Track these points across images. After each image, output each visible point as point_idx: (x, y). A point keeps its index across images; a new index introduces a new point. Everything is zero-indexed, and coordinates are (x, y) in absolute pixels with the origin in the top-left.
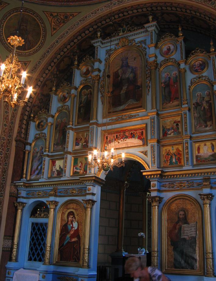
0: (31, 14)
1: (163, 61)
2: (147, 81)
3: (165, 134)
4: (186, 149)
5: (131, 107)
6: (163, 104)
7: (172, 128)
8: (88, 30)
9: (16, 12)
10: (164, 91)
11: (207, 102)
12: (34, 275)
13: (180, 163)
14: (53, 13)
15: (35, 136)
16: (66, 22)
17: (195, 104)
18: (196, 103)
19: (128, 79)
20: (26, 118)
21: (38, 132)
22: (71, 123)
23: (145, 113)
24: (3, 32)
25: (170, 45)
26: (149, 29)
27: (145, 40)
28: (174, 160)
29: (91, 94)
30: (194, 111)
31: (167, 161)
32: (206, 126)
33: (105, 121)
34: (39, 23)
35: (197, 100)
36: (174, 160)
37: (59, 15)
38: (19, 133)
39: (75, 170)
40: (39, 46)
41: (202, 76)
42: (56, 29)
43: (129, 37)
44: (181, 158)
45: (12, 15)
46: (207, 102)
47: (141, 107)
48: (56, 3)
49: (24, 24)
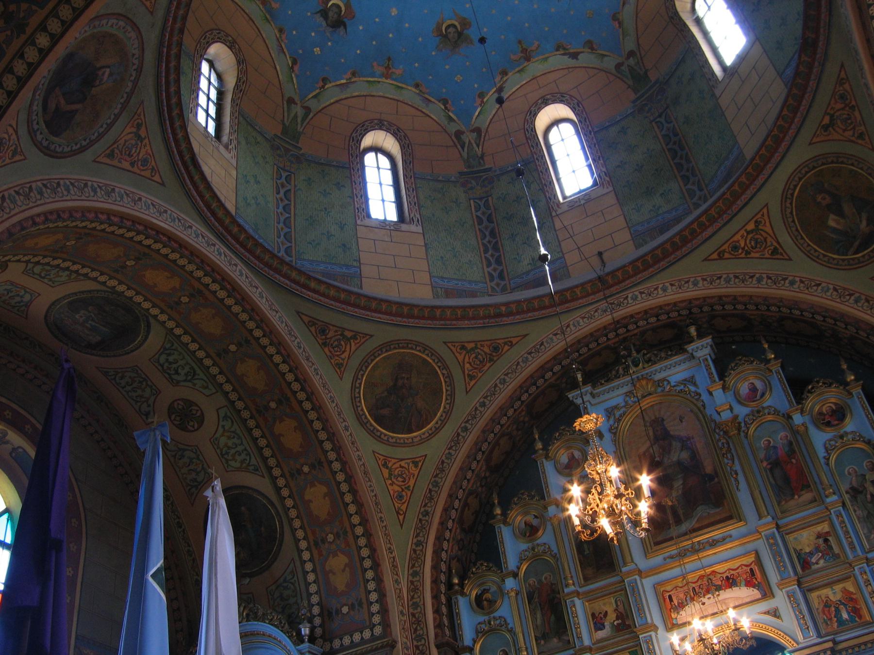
0: (420, 351)
2: (726, 461)
3: (806, 564)
4: (867, 586)
5: (706, 522)
6: (779, 503)
7: (817, 549)
8: (552, 370)
9: (387, 351)
10: (773, 476)
13: (860, 617)
14: (466, 344)
15: (477, 628)
16: (495, 359)
17: (850, 491)
18: (850, 488)
19: (679, 463)
20: (443, 588)
21: (482, 618)
23: (744, 530)
24: (360, 397)
26: (699, 354)
27: (693, 377)
28: (845, 615)
30: (852, 505)
31: (831, 619)
33: (657, 560)
35: (851, 483)
36: (845, 615)
38: (439, 626)
40: (440, 420)
41: (846, 433)
42: (474, 376)
43: (653, 376)
44: (858, 607)
45: (378, 359)
47: (730, 518)
48: (473, 322)
49: (404, 375)
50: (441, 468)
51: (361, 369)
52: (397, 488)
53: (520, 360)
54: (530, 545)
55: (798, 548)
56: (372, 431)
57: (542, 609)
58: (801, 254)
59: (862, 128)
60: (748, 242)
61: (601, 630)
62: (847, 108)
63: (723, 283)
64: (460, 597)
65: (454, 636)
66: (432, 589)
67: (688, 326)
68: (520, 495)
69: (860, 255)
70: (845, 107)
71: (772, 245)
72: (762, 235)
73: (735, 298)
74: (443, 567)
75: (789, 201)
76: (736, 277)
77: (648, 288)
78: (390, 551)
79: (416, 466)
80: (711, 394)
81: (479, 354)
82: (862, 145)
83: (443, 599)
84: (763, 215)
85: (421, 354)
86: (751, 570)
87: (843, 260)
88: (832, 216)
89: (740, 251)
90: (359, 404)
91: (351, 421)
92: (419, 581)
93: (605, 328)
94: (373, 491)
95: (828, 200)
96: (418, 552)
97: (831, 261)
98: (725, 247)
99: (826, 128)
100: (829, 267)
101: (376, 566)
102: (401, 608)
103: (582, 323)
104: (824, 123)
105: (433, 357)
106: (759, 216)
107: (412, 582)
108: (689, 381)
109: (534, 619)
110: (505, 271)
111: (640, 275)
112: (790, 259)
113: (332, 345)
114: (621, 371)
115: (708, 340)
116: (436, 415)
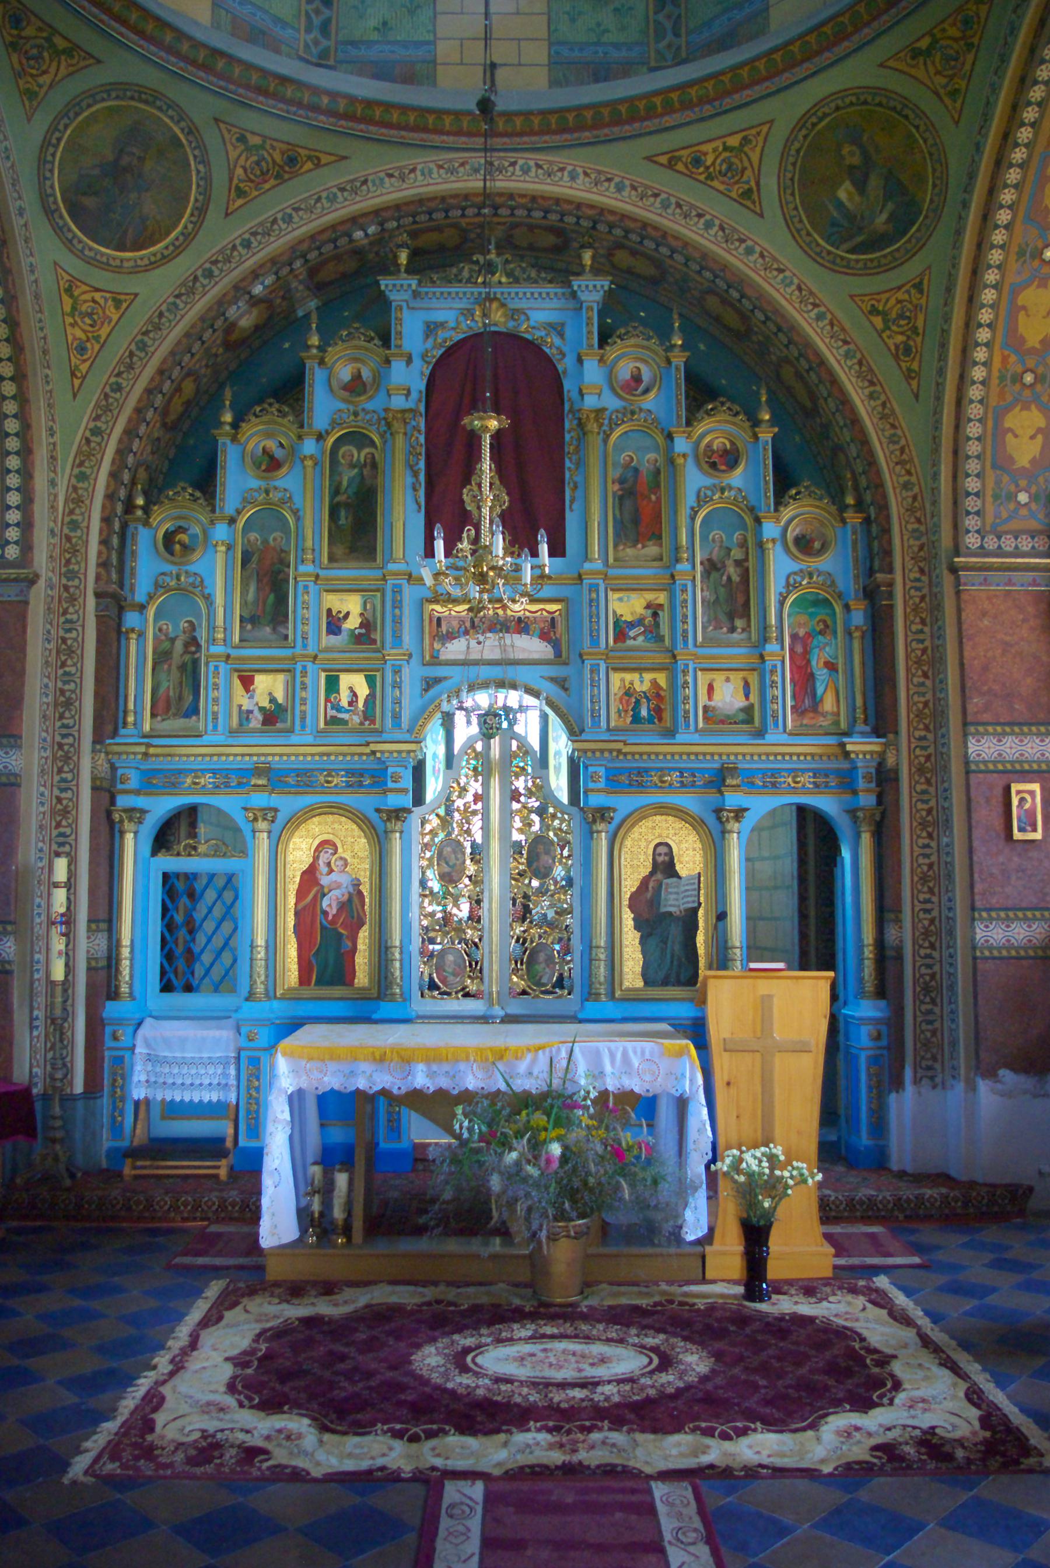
0: (171, 118)
1: (617, 411)
9: (117, 98)
11: (738, 563)
12: (217, 1033)
13: (660, 719)
14: (248, 135)
20: (119, 508)
22: (310, 557)
24: (53, 163)
25: (638, 365)
27: (563, 325)
28: (644, 712)
29: (374, 465)
31: (626, 711)
32: (732, 630)
34: (191, 158)
36: (644, 712)
37: (268, 147)
38: (104, 565)
39: (332, 713)
41: (730, 488)
42: (245, 192)
46: (738, 563)
49: (134, 150)
50: (156, 325)
51: (67, 115)
52: (79, 334)
53: (324, 195)
54: (263, 484)
55: (619, 612)
56: (61, 229)
57: (259, 581)
58: (779, 212)
59: (963, 84)
60: (718, 161)
61: (335, 634)
62: (962, 43)
63: (658, 205)
64: (141, 528)
65: (121, 586)
66: (104, 507)
67: (583, 247)
68: (266, 406)
69: (854, 257)
70: (962, 39)
71: (748, 182)
72: (741, 161)
73: (665, 235)
74: (126, 477)
75: (804, 132)
76: (679, 205)
77: (551, 163)
78: (52, 432)
79: (117, 307)
80: (580, 361)
81: (264, 159)
82: (946, 107)
83: (117, 526)
84: (758, 134)
85: (171, 124)
86: (553, 619)
87: (829, 253)
88: (847, 185)
89: (701, 170)
90: (48, 175)
91: (30, 199)
92: (86, 490)
93: (466, 197)
94: (42, 329)
95: (856, 160)
96: (93, 445)
97: (813, 245)
98: (684, 153)
99: (916, 54)
100: (806, 252)
101: (26, 452)
102: (52, 524)
103: (435, 175)
104: (918, 45)
105: (191, 138)
106: (754, 132)
107: (75, 489)
108: (555, 329)
109: (244, 592)
110: (334, 22)
111: (547, 138)
112: (761, 216)
113: (26, 52)
114: (466, 274)
115: (604, 283)
116: (168, 234)
